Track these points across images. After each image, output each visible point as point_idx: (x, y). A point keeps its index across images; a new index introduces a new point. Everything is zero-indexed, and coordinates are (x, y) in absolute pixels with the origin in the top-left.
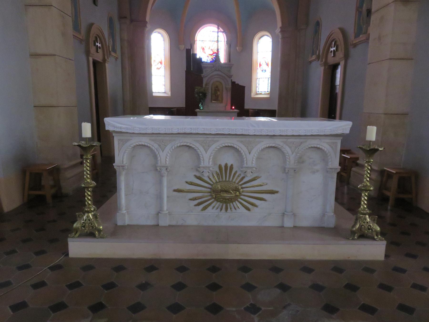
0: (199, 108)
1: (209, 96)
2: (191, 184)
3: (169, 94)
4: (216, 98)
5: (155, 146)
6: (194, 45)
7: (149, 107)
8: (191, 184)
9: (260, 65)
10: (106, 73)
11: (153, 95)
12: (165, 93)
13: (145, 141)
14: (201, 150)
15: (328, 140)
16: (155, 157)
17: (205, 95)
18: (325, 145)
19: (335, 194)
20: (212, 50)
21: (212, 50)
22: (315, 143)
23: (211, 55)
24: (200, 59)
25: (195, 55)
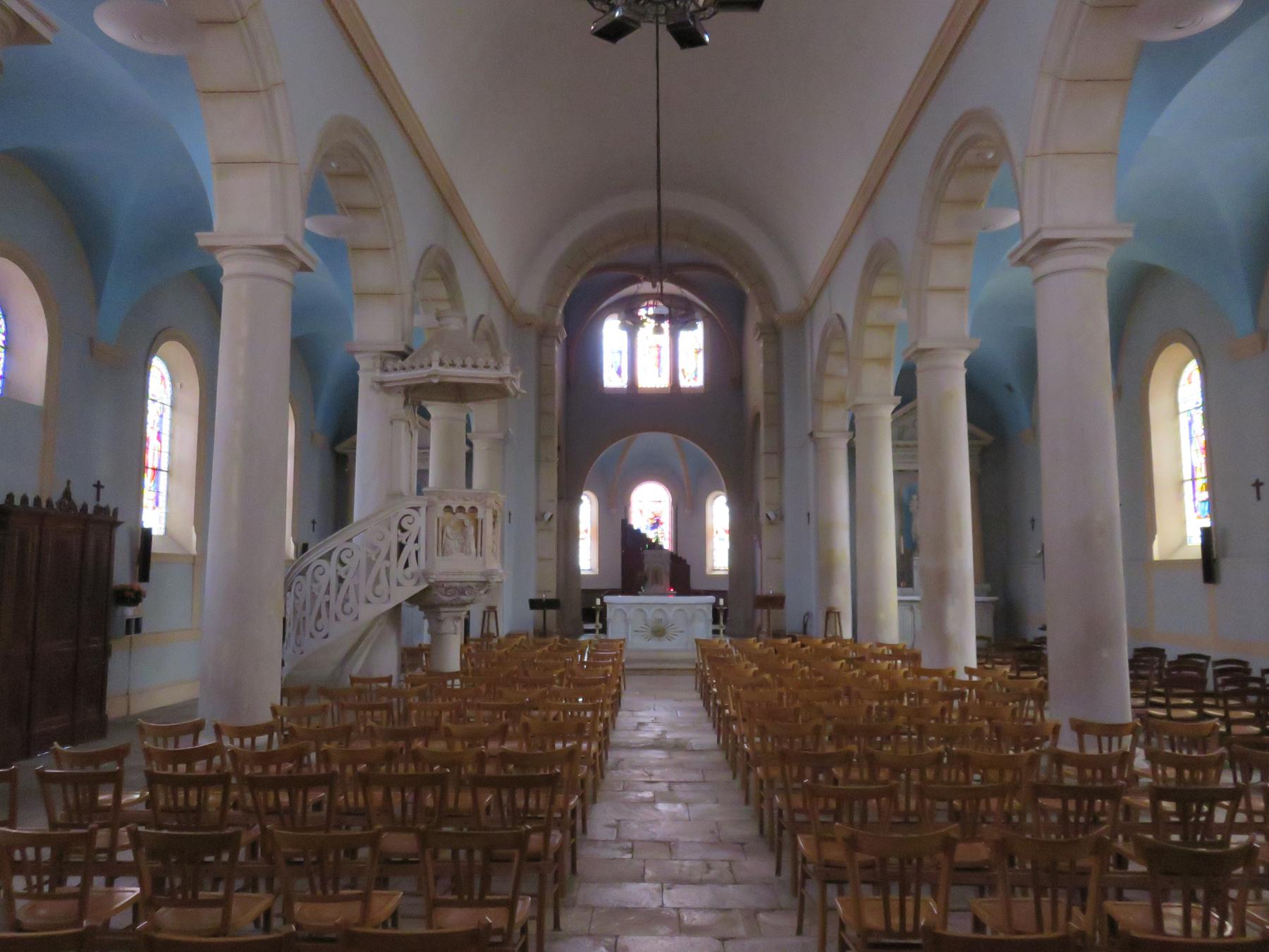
0: (641, 590)
1: (650, 580)
2: (642, 628)
3: (596, 572)
4: (657, 579)
5: (624, 609)
6: (628, 508)
7: (584, 588)
8: (642, 628)
9: (717, 532)
10: (353, 484)
11: (1177, 804)
12: (590, 570)
13: (620, 607)
14: (647, 611)
15: (475, 584)
16: (626, 614)
17: (646, 579)
18: (705, 608)
19: (47, 338)
20: (653, 513)
21: (653, 513)
22: (698, 607)
23: (652, 519)
24: (638, 531)
25: (631, 527)
